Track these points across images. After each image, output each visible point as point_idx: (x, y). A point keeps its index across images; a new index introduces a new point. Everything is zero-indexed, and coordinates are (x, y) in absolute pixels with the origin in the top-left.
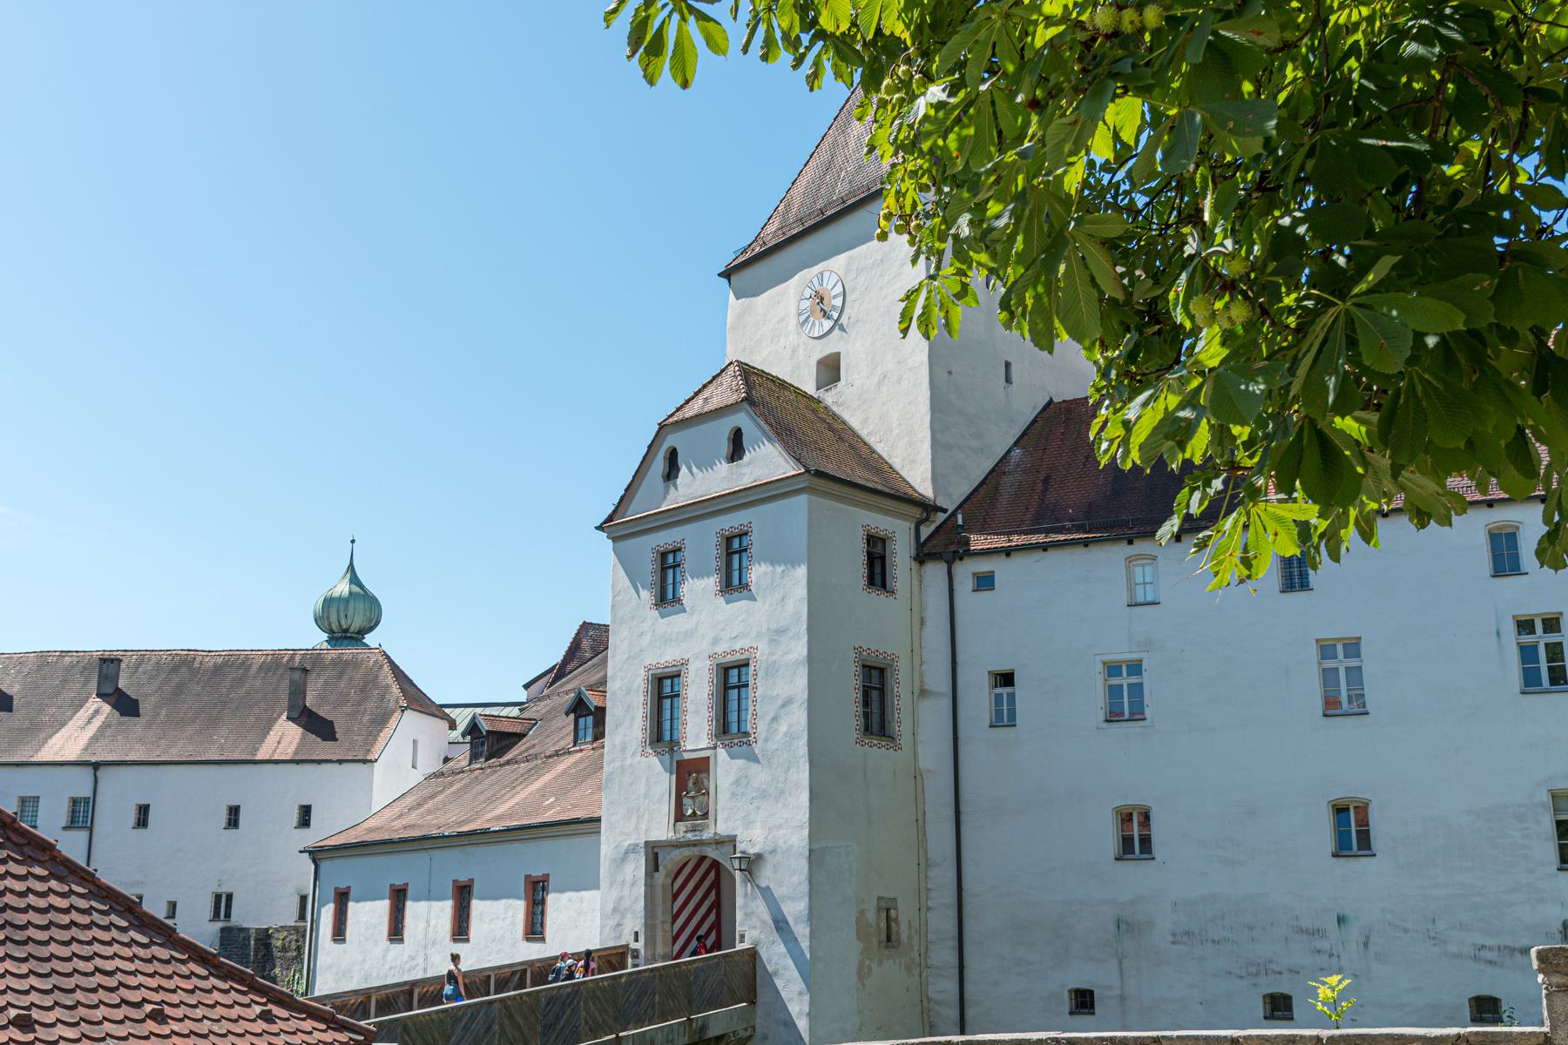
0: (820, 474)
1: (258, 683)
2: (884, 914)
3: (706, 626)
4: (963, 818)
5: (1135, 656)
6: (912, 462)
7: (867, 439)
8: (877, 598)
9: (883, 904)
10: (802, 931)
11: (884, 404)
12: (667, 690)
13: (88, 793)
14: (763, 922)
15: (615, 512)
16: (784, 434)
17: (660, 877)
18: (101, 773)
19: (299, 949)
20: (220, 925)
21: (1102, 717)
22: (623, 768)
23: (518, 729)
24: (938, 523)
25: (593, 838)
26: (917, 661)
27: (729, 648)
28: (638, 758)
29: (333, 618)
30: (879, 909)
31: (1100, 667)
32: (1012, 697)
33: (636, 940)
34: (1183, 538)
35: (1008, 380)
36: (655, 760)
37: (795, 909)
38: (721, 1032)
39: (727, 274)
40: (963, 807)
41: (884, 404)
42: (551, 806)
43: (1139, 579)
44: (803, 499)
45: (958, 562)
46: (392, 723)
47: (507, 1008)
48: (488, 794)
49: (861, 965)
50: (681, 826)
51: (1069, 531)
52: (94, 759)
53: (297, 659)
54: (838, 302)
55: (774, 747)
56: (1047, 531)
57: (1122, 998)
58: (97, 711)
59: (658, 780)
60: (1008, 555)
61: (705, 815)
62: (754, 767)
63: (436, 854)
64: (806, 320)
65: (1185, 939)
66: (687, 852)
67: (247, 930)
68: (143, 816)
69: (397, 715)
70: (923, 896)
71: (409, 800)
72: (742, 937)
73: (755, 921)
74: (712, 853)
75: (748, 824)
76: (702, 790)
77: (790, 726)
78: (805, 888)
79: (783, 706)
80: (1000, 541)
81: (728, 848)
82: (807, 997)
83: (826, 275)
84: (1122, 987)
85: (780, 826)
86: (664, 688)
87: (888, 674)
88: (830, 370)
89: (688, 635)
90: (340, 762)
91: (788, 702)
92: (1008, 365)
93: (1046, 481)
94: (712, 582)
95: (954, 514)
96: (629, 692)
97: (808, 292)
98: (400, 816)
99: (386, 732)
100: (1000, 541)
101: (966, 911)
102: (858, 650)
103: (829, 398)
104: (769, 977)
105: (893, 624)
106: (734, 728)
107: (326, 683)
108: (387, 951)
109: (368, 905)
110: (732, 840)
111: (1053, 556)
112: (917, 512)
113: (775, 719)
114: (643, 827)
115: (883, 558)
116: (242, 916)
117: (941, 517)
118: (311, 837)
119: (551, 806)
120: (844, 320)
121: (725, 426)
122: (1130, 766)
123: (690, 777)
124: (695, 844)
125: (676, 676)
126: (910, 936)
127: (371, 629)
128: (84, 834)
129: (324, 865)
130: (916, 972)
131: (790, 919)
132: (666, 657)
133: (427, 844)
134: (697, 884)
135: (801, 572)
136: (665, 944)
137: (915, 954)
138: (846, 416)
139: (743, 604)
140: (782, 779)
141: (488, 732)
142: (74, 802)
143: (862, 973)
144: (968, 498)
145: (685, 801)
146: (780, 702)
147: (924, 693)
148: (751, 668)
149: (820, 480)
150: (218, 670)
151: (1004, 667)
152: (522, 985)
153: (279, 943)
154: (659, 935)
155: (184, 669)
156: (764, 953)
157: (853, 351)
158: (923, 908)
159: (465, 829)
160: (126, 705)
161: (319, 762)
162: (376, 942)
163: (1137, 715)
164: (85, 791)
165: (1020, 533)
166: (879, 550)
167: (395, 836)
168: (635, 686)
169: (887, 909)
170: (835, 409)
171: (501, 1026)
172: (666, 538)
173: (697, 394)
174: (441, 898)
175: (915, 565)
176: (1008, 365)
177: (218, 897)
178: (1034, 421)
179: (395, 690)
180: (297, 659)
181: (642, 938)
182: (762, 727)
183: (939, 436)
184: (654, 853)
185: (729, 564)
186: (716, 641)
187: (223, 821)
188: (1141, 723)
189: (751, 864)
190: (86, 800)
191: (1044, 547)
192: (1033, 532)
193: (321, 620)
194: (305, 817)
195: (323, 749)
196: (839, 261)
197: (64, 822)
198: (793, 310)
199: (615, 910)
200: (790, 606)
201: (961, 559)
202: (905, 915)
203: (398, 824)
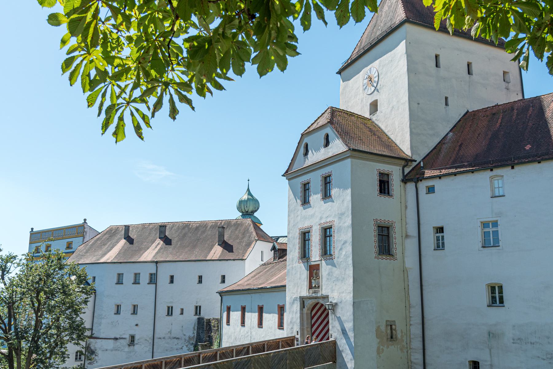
0: (354, 150)
2: (389, 327)
3: (320, 213)
4: (424, 288)
5: (495, 219)
6: (403, 141)
7: (387, 134)
8: (384, 199)
9: (389, 323)
10: (351, 334)
11: (393, 119)
12: (328, 233)
13: (155, 272)
14: (338, 330)
15: (288, 169)
16: (344, 135)
17: (305, 310)
18: (159, 265)
19: (218, 326)
20: (197, 317)
21: (480, 245)
22: (292, 268)
24: (413, 166)
25: (283, 293)
26: (404, 223)
27: (325, 220)
28: (297, 264)
29: (243, 208)
30: (387, 325)
31: (479, 224)
32: (443, 237)
33: (298, 334)
34: (515, 167)
35: (447, 104)
36: (302, 265)
37: (349, 326)
39: (339, 73)
41: (393, 119)
43: (496, 186)
44: (349, 160)
45: (420, 182)
46: (252, 246)
47: (217, 367)
49: (378, 349)
50: (311, 291)
51: (466, 167)
53: (223, 223)
54: (376, 79)
55: (341, 260)
56: (456, 168)
57: (491, 365)
58: (159, 243)
60: (440, 178)
62: (334, 268)
63: (253, 295)
64: (366, 88)
65: (518, 341)
69: (254, 243)
70: (408, 320)
72: (331, 335)
73: (335, 329)
74: (321, 301)
75: (332, 291)
76: (317, 275)
77: (346, 252)
78: (352, 317)
79: (344, 244)
80: (436, 173)
81: (326, 300)
82: (353, 361)
83: (372, 69)
84: (491, 361)
86: (305, 236)
87: (390, 229)
88: (374, 107)
89: (312, 216)
90: (234, 260)
91: (345, 242)
92: (446, 98)
93: (460, 146)
94: (319, 196)
95: (420, 162)
96: (294, 238)
97: (366, 76)
98: (248, 280)
99: (250, 249)
100: (436, 173)
101: (426, 326)
102: (376, 220)
103: (374, 118)
104: (341, 352)
105: (394, 210)
106: (329, 253)
107: (232, 232)
108: (241, 329)
109: (236, 313)
110: (327, 297)
111: (459, 178)
112: (403, 163)
113: (341, 249)
114: (299, 291)
115: (388, 182)
117: (415, 164)
120: (378, 87)
121: (321, 135)
122: (493, 267)
123: (314, 271)
126: (402, 336)
127: (256, 211)
128: (154, 285)
129: (224, 297)
130: (405, 351)
131: (347, 329)
132: (306, 225)
133: (250, 292)
134: (318, 313)
135: (349, 191)
137: (405, 343)
138: (380, 125)
139: (330, 203)
140: (343, 273)
142: (151, 274)
143: (379, 351)
144: (428, 155)
145: (313, 281)
146: (342, 243)
147: (407, 236)
149: (355, 153)
150: (197, 228)
151: (440, 225)
152: (248, 353)
153: (213, 324)
154: (306, 332)
157: (382, 98)
159: (260, 287)
160: (167, 241)
161: (227, 260)
163: (496, 245)
164: (154, 271)
165: (445, 169)
166: (385, 178)
169: (391, 326)
170: (376, 122)
172: (304, 179)
173: (315, 121)
174: (255, 312)
175: (402, 184)
176: (446, 98)
177: (196, 307)
178: (460, 121)
179: (254, 234)
180: (223, 223)
181: (299, 333)
183: (413, 130)
184: (303, 300)
186: (321, 218)
187: (197, 281)
188: (497, 248)
189: (334, 306)
191: (455, 174)
192: (451, 168)
193: (239, 208)
196: (376, 63)
197: (148, 281)
198: (361, 85)
199: (291, 322)
200: (345, 204)
201: (421, 181)
202: (400, 327)
203: (246, 283)
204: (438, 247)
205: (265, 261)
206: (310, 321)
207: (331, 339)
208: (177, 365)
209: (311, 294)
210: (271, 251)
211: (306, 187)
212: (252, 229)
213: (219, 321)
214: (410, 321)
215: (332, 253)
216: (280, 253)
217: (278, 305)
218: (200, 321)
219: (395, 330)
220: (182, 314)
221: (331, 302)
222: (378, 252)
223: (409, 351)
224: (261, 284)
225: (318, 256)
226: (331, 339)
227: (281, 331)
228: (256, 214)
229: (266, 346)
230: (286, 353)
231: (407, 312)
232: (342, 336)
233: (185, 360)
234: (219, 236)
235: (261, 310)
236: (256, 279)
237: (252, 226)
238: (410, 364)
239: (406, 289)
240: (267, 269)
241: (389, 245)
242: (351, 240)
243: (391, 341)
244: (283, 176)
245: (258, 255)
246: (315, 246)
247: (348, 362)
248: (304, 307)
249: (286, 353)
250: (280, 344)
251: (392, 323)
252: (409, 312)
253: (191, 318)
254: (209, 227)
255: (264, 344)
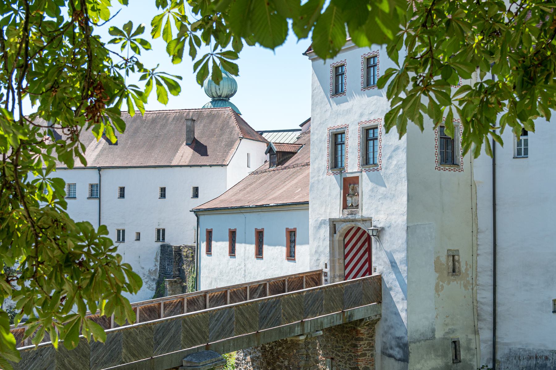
1: (172, 127)
4: (498, 207)
9: (451, 253)
10: (403, 268)
13: (98, 182)
14: (385, 262)
17: (337, 237)
19: (193, 257)
20: (160, 244)
23: (292, 150)
29: (213, 91)
30: (448, 256)
32: (526, 141)
33: (326, 268)
36: (333, 177)
37: (399, 257)
38: (361, 318)
40: (497, 202)
42: (298, 194)
46: (236, 146)
47: (239, 309)
48: (274, 185)
49: (437, 285)
52: (98, 166)
53: (191, 114)
55: (390, 172)
59: (332, 187)
61: (357, 206)
63: (248, 215)
66: (353, 224)
67: (171, 246)
68: (122, 193)
69: (238, 141)
70: (475, 248)
71: (240, 186)
72: (375, 269)
74: (360, 225)
75: (377, 212)
76: (355, 193)
77: (398, 161)
78: (405, 246)
79: (394, 151)
81: (368, 223)
85: (393, 214)
86: (337, 139)
89: (348, 111)
90: (211, 166)
96: (321, 141)
99: (233, 150)
106: (371, 162)
107: (204, 126)
110: (370, 220)
113: (390, 157)
114: (328, 211)
116: (172, 240)
118: (197, 204)
119: (298, 194)
123: (350, 186)
124: (353, 221)
125: (343, 133)
126: (467, 269)
127: (232, 95)
128: (97, 201)
129: (202, 218)
130: (470, 288)
131: (397, 262)
132: (338, 123)
133: (243, 210)
134: (355, 241)
136: (340, 270)
137: (469, 278)
141: (277, 152)
142: (92, 186)
143: (438, 289)
146: (393, 148)
148: (379, 130)
150: (154, 121)
153: (185, 254)
154: (337, 265)
155: (138, 121)
156: (385, 278)
158: (475, 254)
159: (259, 204)
161: (201, 166)
162: (224, 256)
167: (230, 206)
168: (323, 138)
169: (453, 256)
171: (237, 318)
177: (158, 231)
179: (237, 129)
180: (191, 114)
181: (328, 266)
182: (384, 162)
184: (333, 225)
185: (368, 73)
186: (361, 115)
189: (380, 232)
190: (97, 185)
194: (196, 193)
195: (203, 160)
197: (87, 195)
199: (316, 252)
202: (464, 258)
203: (234, 199)
204: (519, 153)
205: (253, 169)
206: (343, 250)
207: (374, 274)
208: (178, 308)
209: (345, 216)
210: (266, 153)
211: (338, 72)
212: (233, 121)
213: (195, 250)
214: (477, 250)
215: (377, 161)
216: (279, 157)
217: (287, 229)
218: (165, 250)
219: (458, 261)
220: (138, 239)
221: (375, 226)
222: (439, 161)
223: (475, 289)
224: (258, 200)
225: (356, 165)
226: (374, 274)
227: (291, 264)
228: (232, 100)
229: (286, 283)
230: (322, 292)
231: (474, 238)
232: (390, 270)
233: (188, 301)
234: (187, 132)
235: (233, 237)
236: (248, 193)
237: (233, 118)
238: (475, 304)
239: (474, 210)
240: (262, 179)
241: (453, 152)
242: (405, 145)
243: (452, 275)
244: (305, 54)
245: (244, 161)
246: (353, 153)
247: (398, 302)
248: (335, 233)
249: (322, 292)
250: (304, 280)
251: (455, 253)
252: (477, 238)
253: (151, 245)
254: (171, 119)
255: (284, 280)
